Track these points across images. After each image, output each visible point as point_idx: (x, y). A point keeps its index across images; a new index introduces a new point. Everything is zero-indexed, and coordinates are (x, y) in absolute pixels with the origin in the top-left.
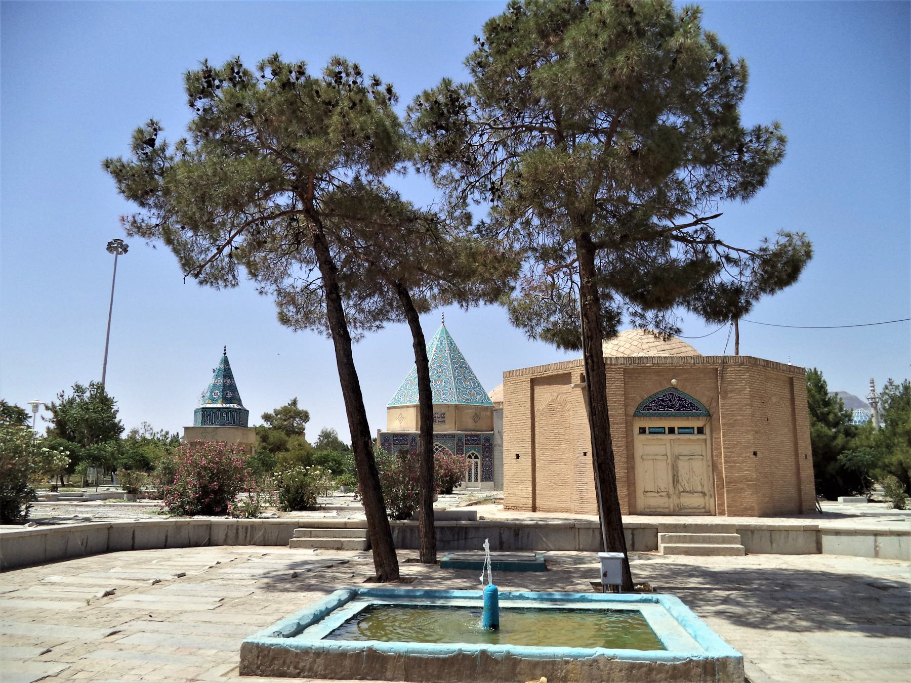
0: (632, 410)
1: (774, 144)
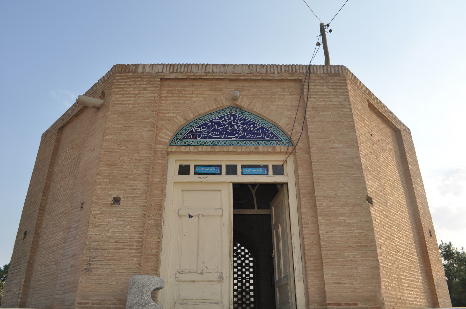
0: (166, 136)
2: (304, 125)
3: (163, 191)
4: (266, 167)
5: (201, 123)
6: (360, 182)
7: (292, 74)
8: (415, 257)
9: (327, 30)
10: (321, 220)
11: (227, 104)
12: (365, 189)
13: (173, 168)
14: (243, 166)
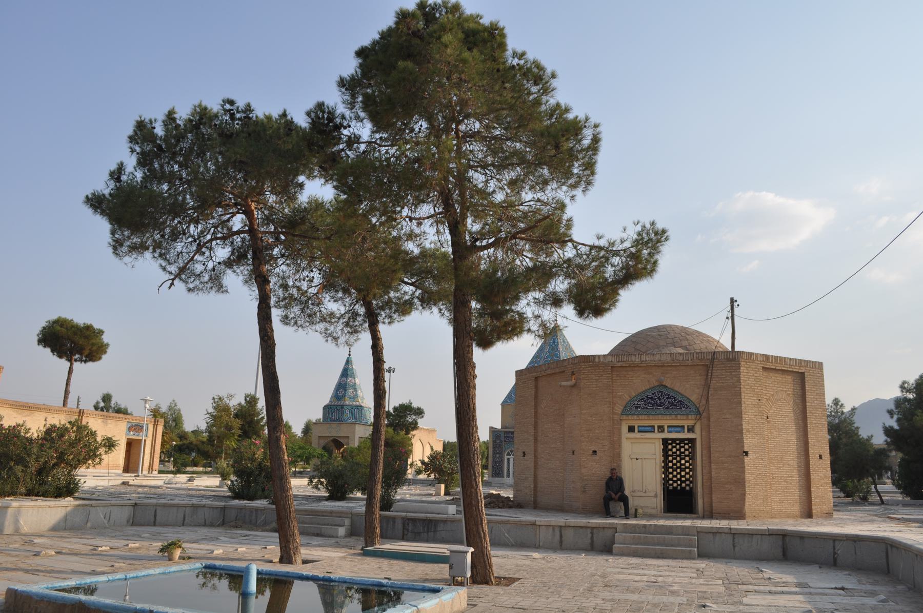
0: (619, 409)
1: (156, 255)
2: (707, 400)
3: (620, 446)
4: (683, 427)
5: (640, 398)
6: (740, 441)
7: (701, 360)
8: (796, 477)
9: (736, 304)
10: (713, 466)
11: (656, 384)
12: (743, 446)
13: (625, 429)
14: (668, 427)
